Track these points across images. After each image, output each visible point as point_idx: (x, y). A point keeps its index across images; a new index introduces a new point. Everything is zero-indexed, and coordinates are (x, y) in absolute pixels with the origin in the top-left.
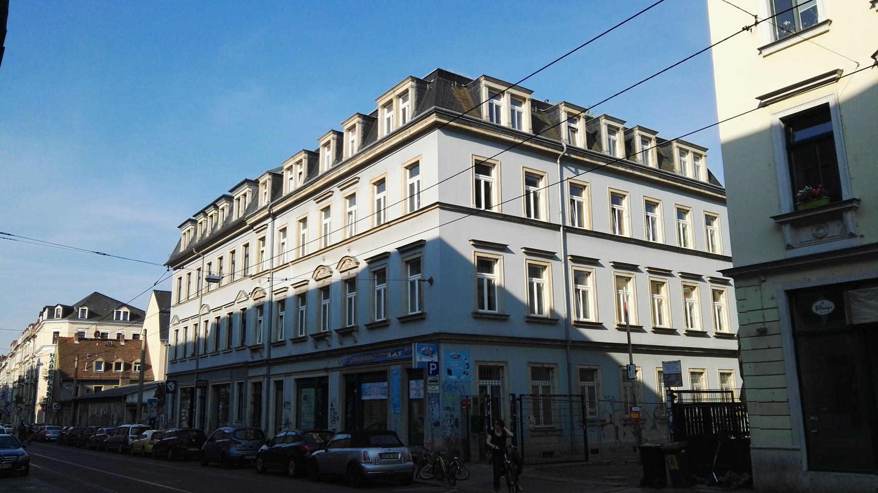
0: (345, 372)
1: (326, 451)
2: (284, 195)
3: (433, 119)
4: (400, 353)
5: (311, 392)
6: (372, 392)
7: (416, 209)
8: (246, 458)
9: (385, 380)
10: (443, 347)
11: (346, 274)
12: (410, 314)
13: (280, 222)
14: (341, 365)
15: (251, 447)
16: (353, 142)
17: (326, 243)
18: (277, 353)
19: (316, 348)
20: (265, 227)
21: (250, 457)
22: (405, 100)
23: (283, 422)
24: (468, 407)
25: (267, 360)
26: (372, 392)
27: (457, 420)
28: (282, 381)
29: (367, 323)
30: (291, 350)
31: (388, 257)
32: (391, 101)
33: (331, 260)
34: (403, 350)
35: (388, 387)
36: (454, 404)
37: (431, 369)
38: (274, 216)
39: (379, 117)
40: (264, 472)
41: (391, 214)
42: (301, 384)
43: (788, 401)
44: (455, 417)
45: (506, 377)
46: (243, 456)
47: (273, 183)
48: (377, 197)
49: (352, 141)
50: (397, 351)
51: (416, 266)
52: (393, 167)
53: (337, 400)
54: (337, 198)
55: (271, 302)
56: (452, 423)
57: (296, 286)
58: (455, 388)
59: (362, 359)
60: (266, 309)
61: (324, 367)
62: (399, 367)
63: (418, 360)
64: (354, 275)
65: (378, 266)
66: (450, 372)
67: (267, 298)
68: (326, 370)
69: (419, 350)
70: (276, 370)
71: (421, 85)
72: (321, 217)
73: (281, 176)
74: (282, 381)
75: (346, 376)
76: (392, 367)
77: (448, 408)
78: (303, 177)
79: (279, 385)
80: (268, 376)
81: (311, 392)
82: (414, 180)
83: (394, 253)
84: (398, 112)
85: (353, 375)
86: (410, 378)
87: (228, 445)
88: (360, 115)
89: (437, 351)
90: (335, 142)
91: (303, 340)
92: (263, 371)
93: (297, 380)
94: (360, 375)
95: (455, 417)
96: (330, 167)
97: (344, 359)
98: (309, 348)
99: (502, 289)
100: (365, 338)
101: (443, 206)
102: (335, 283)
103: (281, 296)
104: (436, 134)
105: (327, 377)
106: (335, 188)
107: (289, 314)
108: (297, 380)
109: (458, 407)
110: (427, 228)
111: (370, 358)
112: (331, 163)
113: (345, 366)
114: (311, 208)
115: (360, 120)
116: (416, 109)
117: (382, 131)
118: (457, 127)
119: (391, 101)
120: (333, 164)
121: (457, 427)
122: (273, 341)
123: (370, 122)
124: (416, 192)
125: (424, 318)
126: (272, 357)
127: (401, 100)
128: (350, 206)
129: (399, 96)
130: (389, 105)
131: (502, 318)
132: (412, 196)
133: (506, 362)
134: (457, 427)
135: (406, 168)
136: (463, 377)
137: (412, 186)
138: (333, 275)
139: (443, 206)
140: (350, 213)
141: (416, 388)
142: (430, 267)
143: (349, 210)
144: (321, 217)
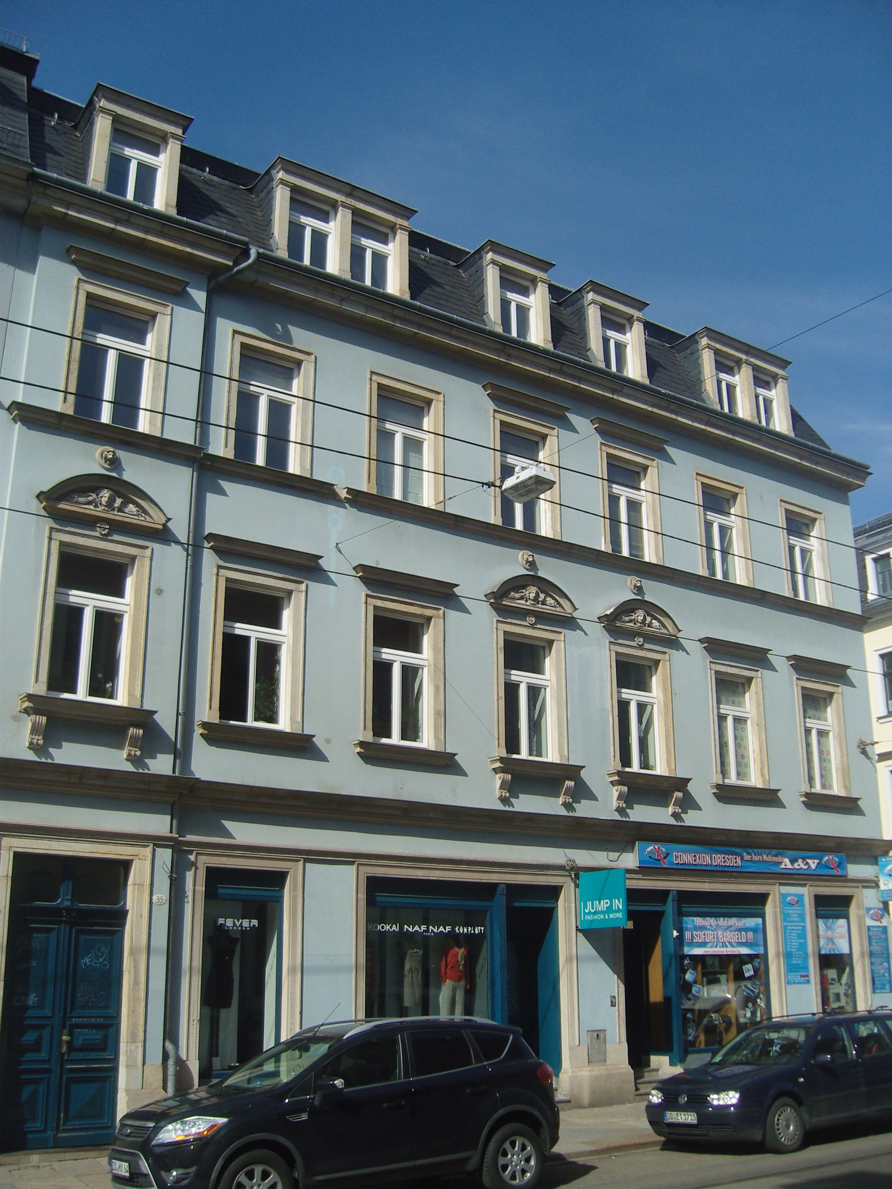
26: (712, 937)
34: (820, 859)
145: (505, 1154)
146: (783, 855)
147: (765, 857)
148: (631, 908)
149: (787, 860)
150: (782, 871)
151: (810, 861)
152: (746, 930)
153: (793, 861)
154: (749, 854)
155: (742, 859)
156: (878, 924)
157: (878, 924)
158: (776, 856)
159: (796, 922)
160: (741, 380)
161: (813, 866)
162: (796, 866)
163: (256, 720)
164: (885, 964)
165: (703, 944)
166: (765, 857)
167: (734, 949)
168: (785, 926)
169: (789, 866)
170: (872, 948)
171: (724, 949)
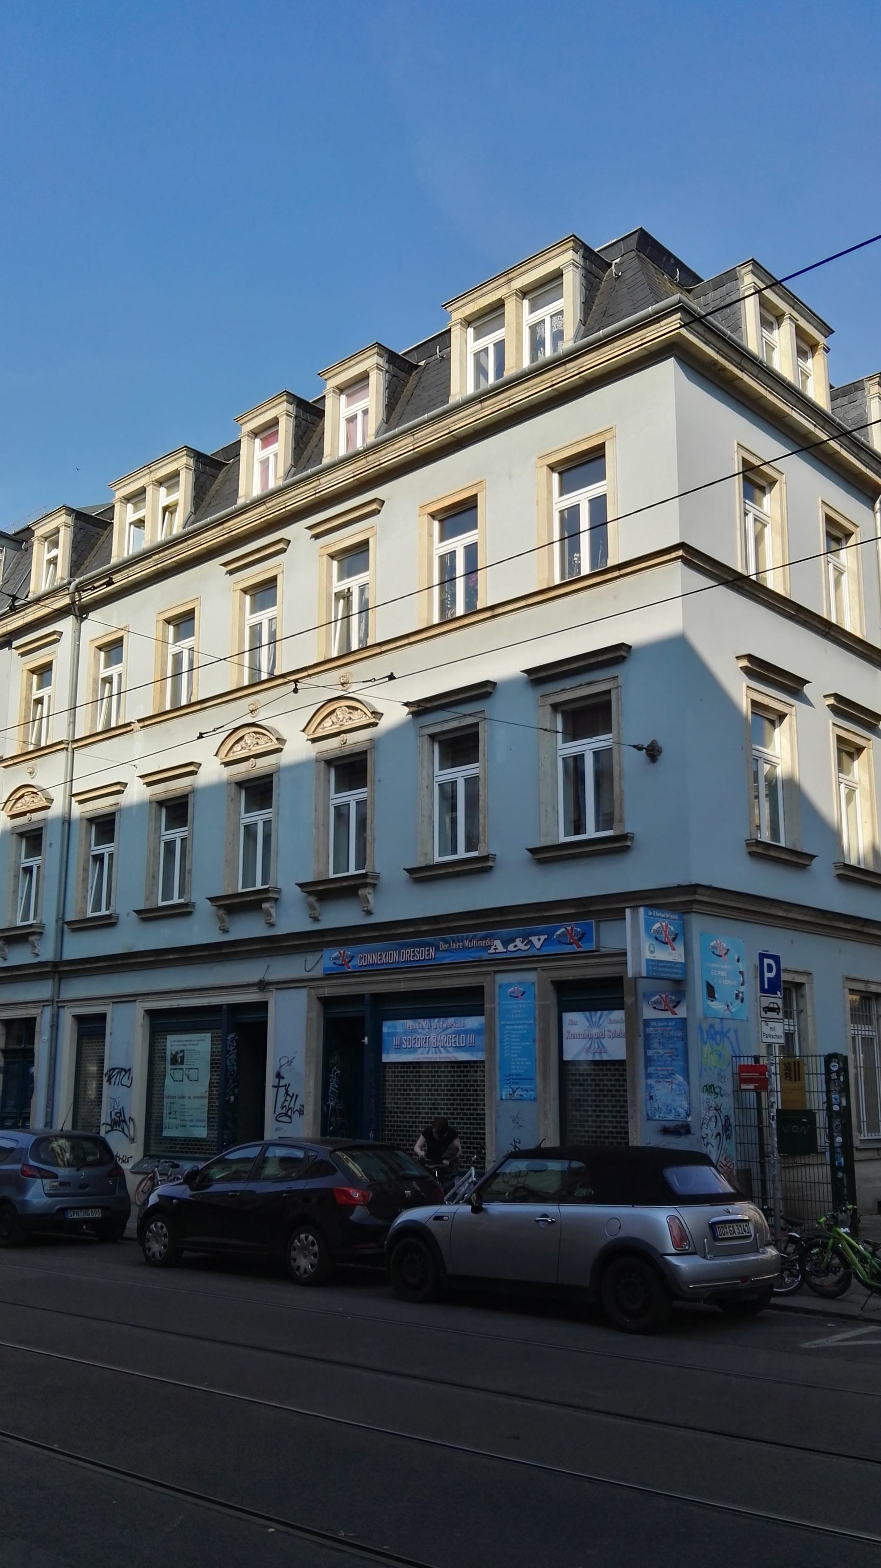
0: (327, 992)
1: (477, 1210)
2: (241, 501)
3: (671, 325)
4: (537, 941)
5: (199, 1047)
6: (417, 1042)
7: (184, 702)
8: (72, 1215)
9: (479, 1011)
10: (697, 924)
11: (333, 744)
12: (161, 904)
13: (98, 626)
14: (318, 972)
15: (83, 1186)
16: (352, 420)
17: (255, 669)
18: (80, 947)
19: (316, 919)
20: (55, 639)
21: (81, 1215)
22: (266, 443)
23: (105, 1118)
24: (762, 1084)
25: (55, 964)
26: (417, 1042)
27: (727, 1118)
28: (102, 1017)
29: (142, 907)
30: (130, 937)
31: (487, 695)
32: (142, 491)
33: (49, 775)
34: (550, 933)
35: (488, 1030)
36: (721, 1077)
37: (767, 975)
38: (81, 611)
39: (116, 522)
40: (172, 1261)
41: (207, 684)
42: (162, 1022)
43: (535, 1099)
44: (724, 1112)
45: (809, 1011)
46: (63, 1210)
47: (297, 426)
48: (251, 619)
49: (353, 421)
50: (526, 937)
51: (588, 717)
52: (139, 616)
53: (300, 1062)
54: (304, 563)
55: (67, 821)
56: (720, 1129)
57: (151, 779)
58: (724, 1034)
59: (394, 957)
60: (52, 839)
61: (256, 978)
62: (531, 977)
63: (648, 955)
64: (267, 771)
65: (448, 721)
66: (711, 992)
67: (57, 810)
68: (262, 985)
69: (649, 925)
70: (78, 988)
71: (594, 264)
72: (242, 608)
73: (320, 414)
74: (102, 1017)
75: (326, 1002)
76: (501, 979)
77: (710, 1088)
78: (179, 518)
79: (91, 1028)
80: (57, 1004)
81: (199, 1047)
82: (264, 616)
83: (510, 683)
84: (519, 332)
85: (358, 999)
86: (564, 1007)
87: (20, 1183)
88: (70, 511)
89: (682, 935)
90: (291, 422)
91: (183, 911)
92: (43, 990)
93: (152, 1014)
94: (379, 998)
95: (724, 1112)
96: (371, 440)
97: (329, 958)
98: (201, 930)
99: (791, 784)
100: (399, 903)
101: (692, 557)
102: (130, 808)
103: (102, 805)
104: (669, 369)
105: (263, 1006)
106: (297, 531)
107: (131, 852)
108: (152, 1014)
109: (728, 1087)
110: (646, 613)
111: (394, 957)
112: (281, 472)
113: (329, 976)
114: (213, 590)
115: (292, 408)
116: (584, 322)
117: (124, 543)
118: (715, 363)
119: (142, 491)
120: (287, 475)
121: (729, 1137)
122: (70, 917)
123: (92, 529)
124: (185, 667)
125: (189, 914)
126: (68, 955)
127: (258, 441)
128: (40, 687)
129: (160, 483)
130: (136, 498)
131: (796, 860)
132: (177, 675)
133: (809, 974)
134: (729, 1137)
135: (552, 468)
136: (736, 1005)
137: (177, 658)
138: (286, 748)
139: (692, 557)
140: (39, 701)
141: (592, 1036)
142: (637, 713)
143: (36, 694)
144: (242, 608)
145: (149, 1249)
146: (492, 937)
147: (467, 943)
148: (31, 1046)
149: (498, 943)
150: (492, 957)
151: (534, 939)
152: (467, 1032)
153: (505, 944)
154: (446, 941)
155: (437, 949)
156: (668, 1015)
157: (668, 1015)
158: (484, 938)
159: (520, 1019)
160: (783, 338)
161: (538, 944)
162: (511, 947)
163: (597, 830)
164: (680, 1078)
165: (413, 1050)
166: (467, 943)
167: (449, 1055)
168: (504, 1025)
169: (501, 949)
170: (650, 1053)
171: (437, 1056)
